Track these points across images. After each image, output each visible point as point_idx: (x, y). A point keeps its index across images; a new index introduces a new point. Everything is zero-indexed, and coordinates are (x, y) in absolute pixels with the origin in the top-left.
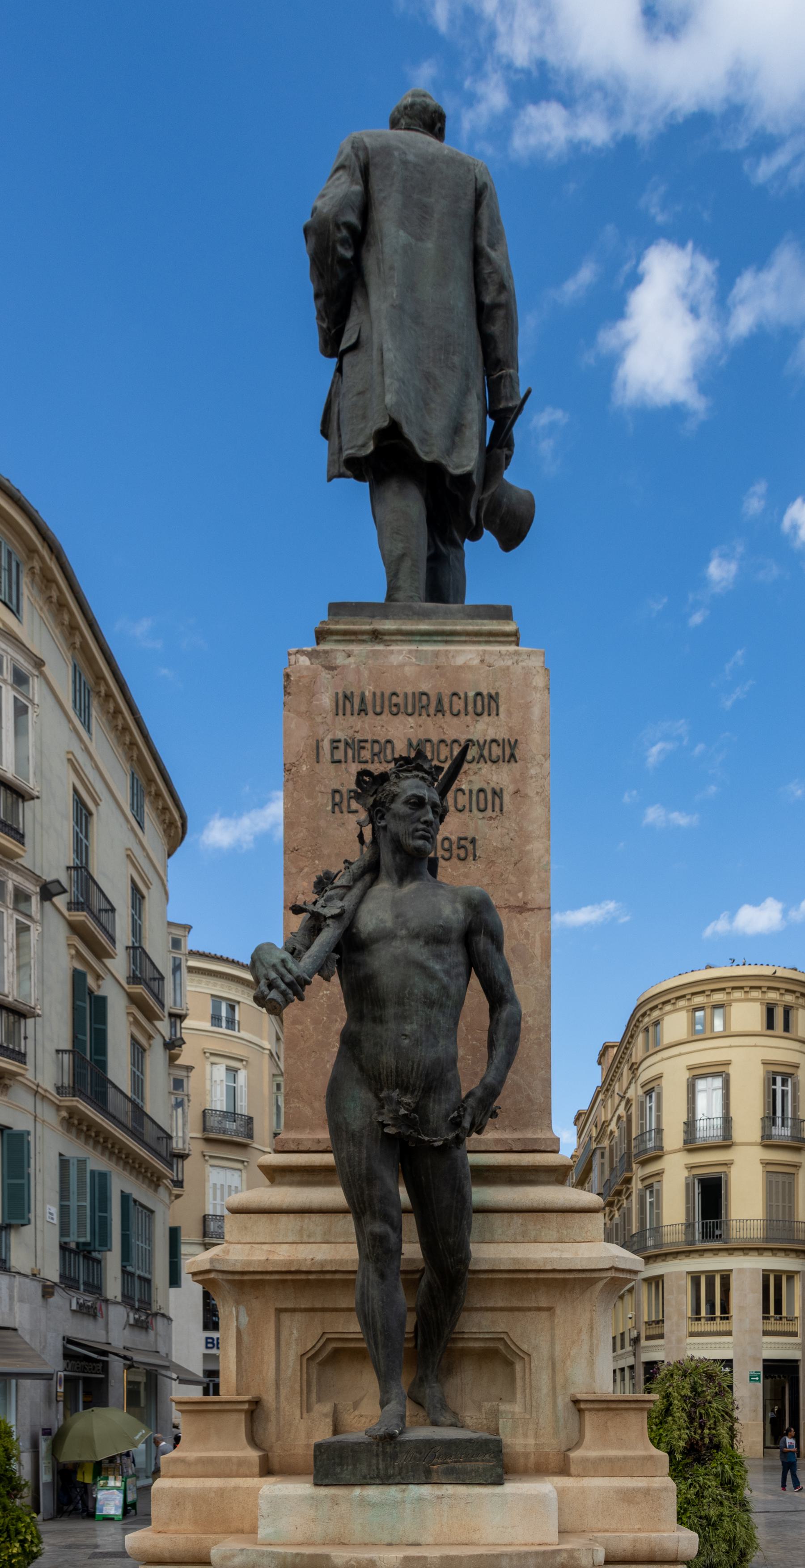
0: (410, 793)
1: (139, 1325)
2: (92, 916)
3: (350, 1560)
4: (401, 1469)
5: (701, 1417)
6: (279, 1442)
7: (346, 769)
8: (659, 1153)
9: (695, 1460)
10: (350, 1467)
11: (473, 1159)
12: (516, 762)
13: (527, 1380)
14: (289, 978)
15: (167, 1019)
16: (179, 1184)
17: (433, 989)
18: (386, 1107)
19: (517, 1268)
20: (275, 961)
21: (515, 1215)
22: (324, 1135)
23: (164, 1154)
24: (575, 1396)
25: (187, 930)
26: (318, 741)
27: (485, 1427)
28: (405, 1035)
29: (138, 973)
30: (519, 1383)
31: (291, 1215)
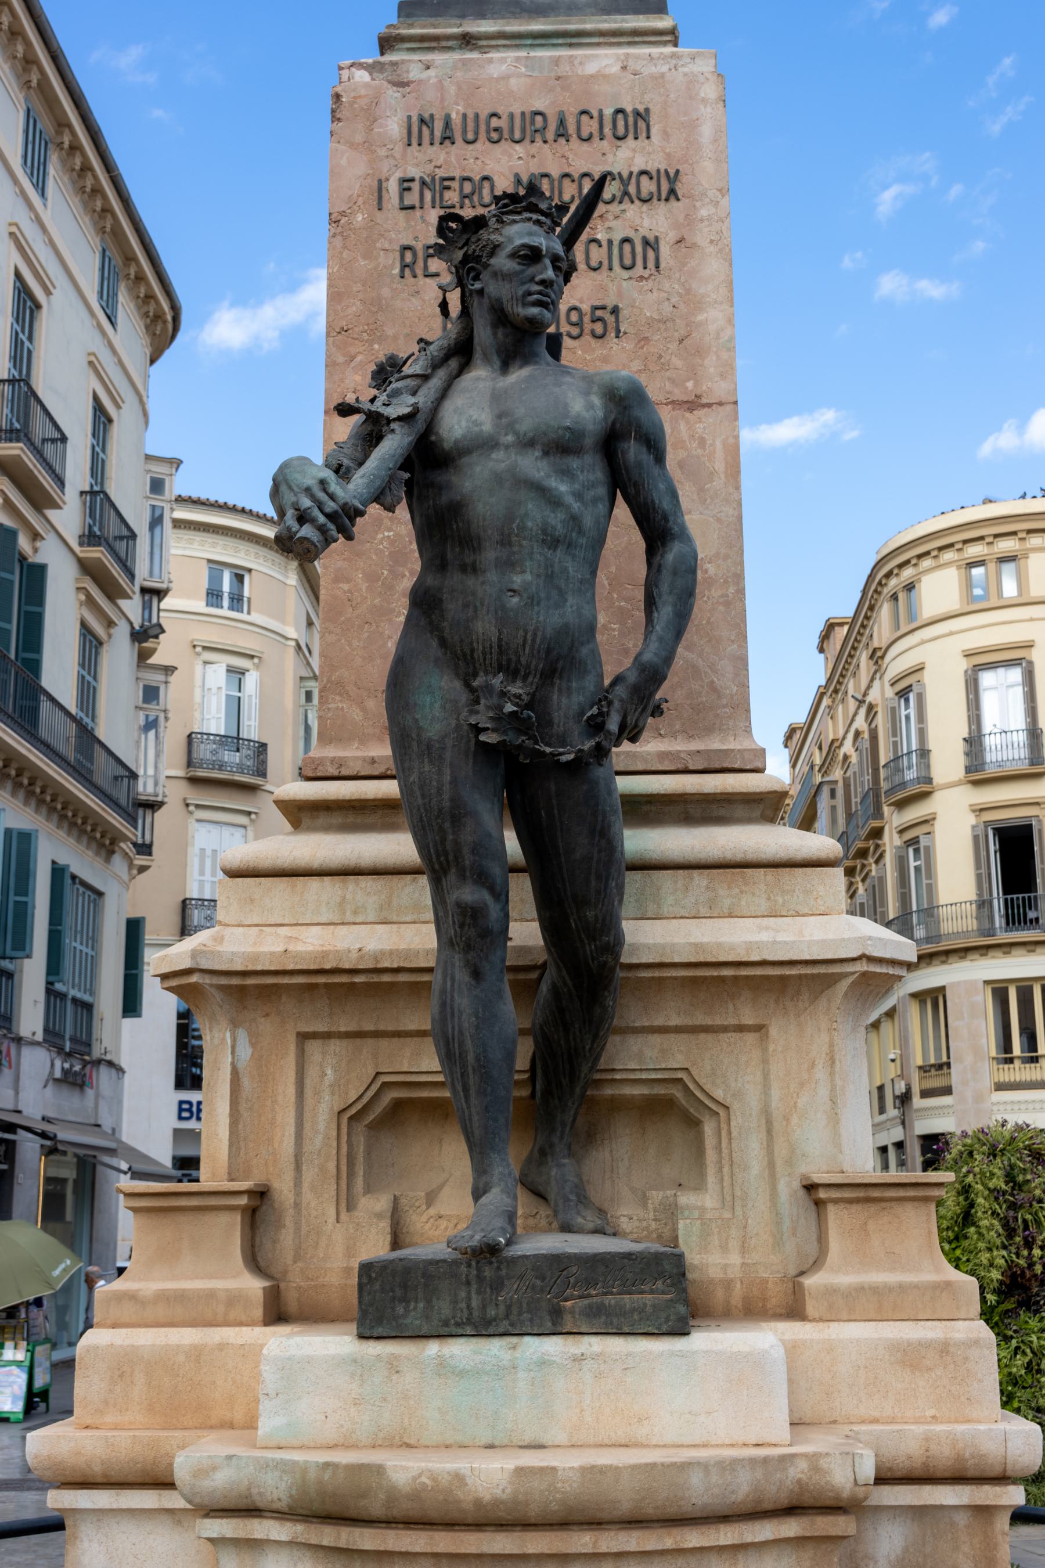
0: (518, 242)
1: (71, 1079)
2: (32, 448)
3: (420, 1475)
4: (509, 1308)
5: (1026, 1227)
6: (299, 1264)
7: (422, 217)
8: (926, 788)
9: (1020, 1304)
10: (421, 1305)
11: (625, 784)
12: (678, 200)
13: (725, 1151)
14: (331, 506)
15: (137, 598)
16: (145, 849)
17: (556, 520)
18: (483, 701)
19: (702, 959)
20: (310, 482)
21: (695, 873)
22: (383, 751)
23: (123, 802)
24: (808, 1178)
25: (175, 466)
26: (380, 181)
27: (654, 1235)
28: (514, 591)
29: (96, 529)
30: (710, 1155)
31: (326, 878)
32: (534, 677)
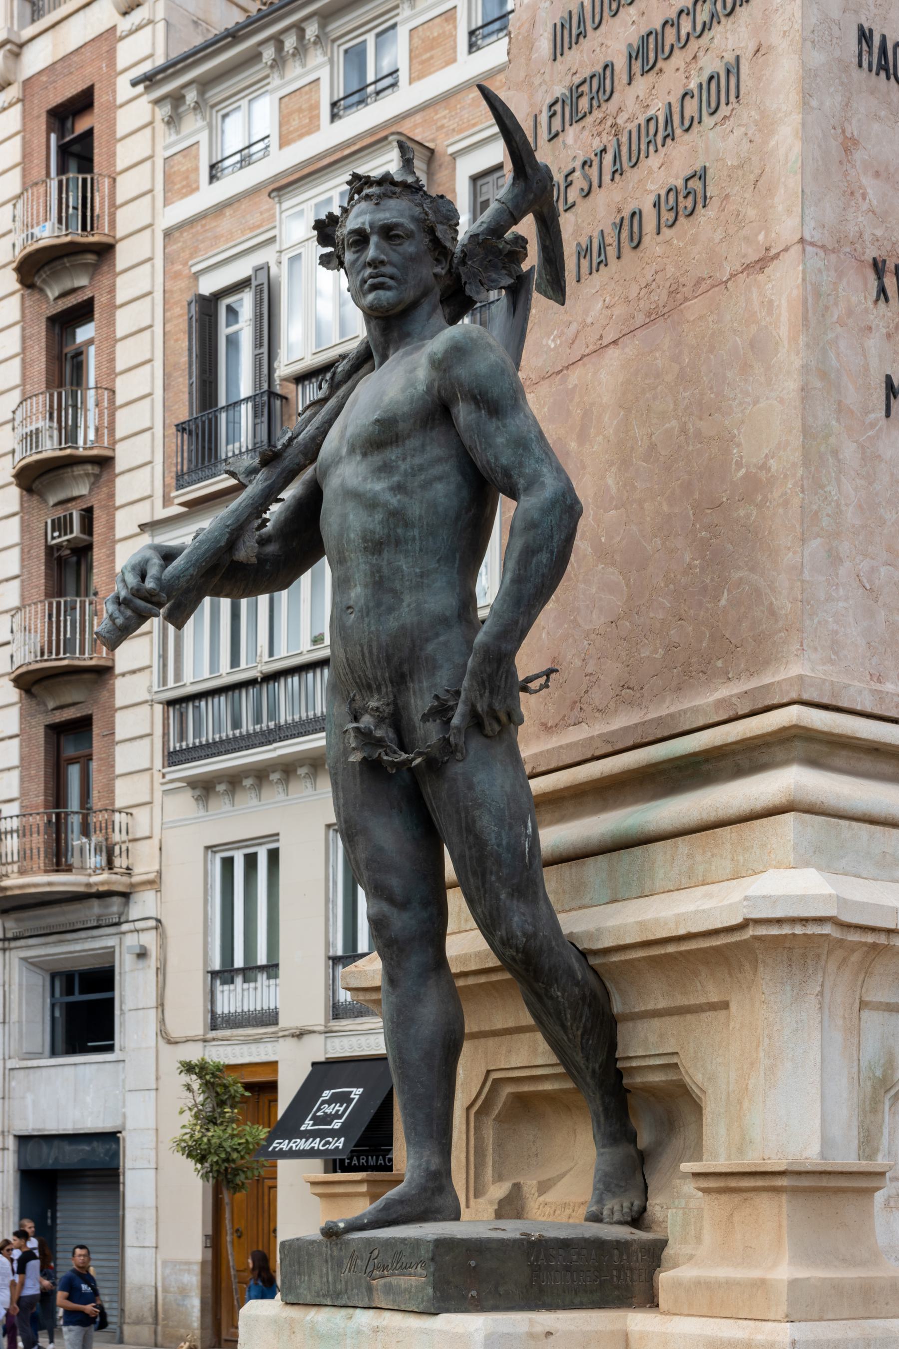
21: (679, 840)
32: (387, 687)
